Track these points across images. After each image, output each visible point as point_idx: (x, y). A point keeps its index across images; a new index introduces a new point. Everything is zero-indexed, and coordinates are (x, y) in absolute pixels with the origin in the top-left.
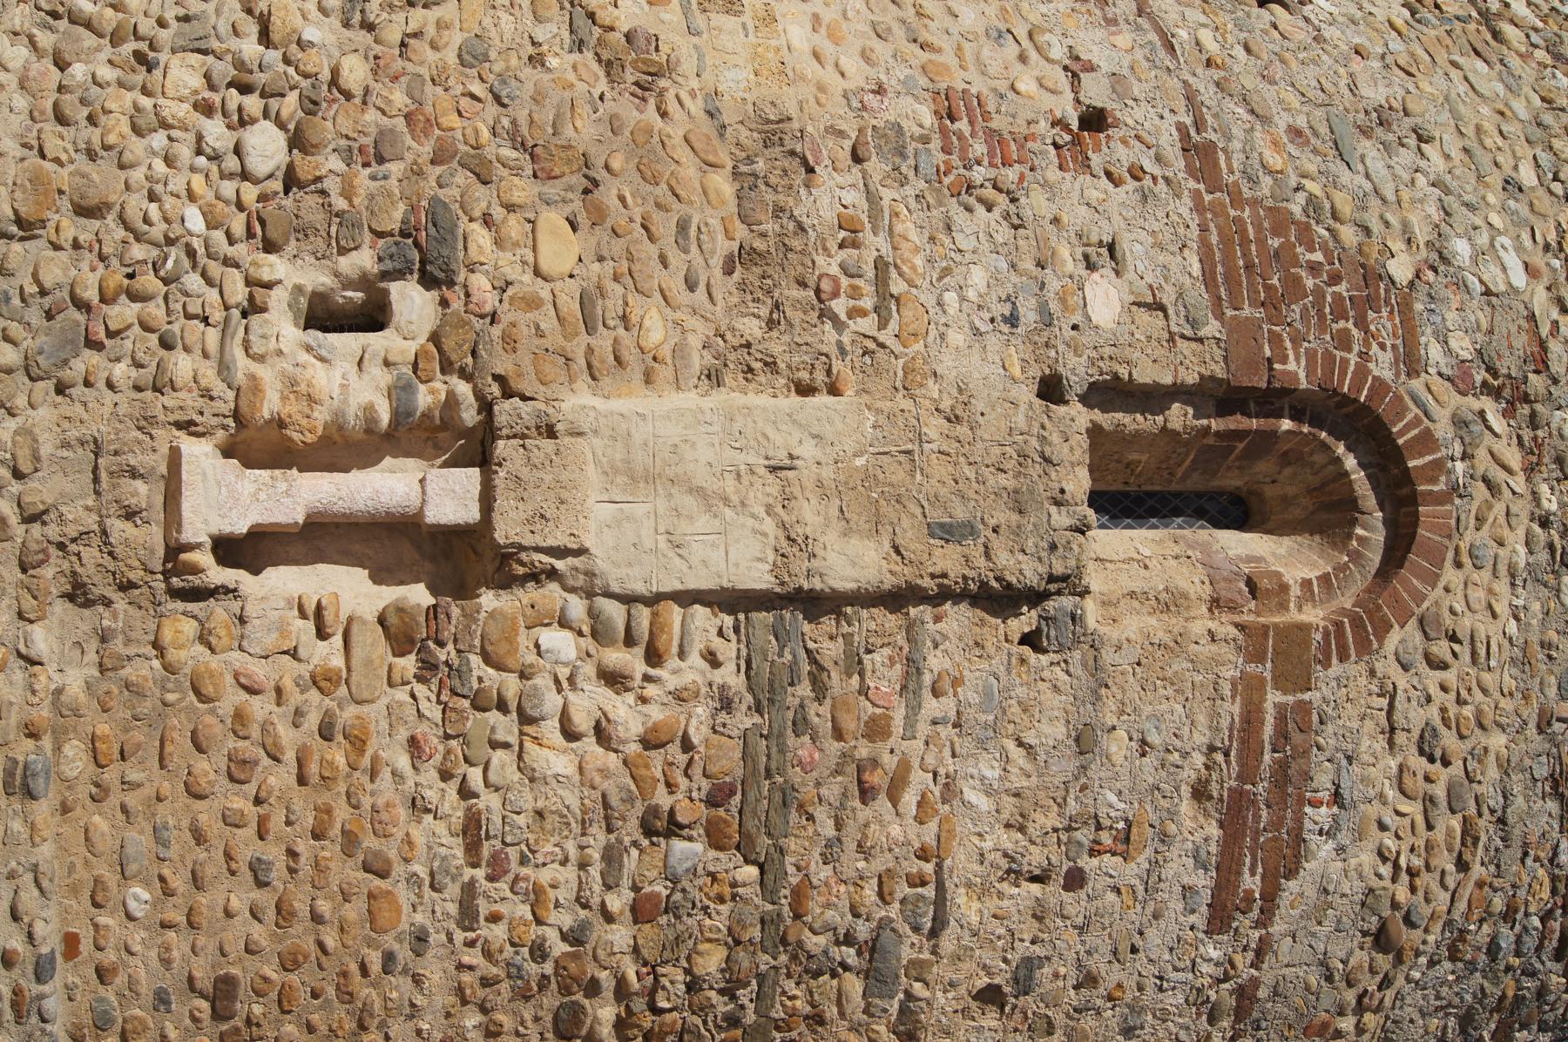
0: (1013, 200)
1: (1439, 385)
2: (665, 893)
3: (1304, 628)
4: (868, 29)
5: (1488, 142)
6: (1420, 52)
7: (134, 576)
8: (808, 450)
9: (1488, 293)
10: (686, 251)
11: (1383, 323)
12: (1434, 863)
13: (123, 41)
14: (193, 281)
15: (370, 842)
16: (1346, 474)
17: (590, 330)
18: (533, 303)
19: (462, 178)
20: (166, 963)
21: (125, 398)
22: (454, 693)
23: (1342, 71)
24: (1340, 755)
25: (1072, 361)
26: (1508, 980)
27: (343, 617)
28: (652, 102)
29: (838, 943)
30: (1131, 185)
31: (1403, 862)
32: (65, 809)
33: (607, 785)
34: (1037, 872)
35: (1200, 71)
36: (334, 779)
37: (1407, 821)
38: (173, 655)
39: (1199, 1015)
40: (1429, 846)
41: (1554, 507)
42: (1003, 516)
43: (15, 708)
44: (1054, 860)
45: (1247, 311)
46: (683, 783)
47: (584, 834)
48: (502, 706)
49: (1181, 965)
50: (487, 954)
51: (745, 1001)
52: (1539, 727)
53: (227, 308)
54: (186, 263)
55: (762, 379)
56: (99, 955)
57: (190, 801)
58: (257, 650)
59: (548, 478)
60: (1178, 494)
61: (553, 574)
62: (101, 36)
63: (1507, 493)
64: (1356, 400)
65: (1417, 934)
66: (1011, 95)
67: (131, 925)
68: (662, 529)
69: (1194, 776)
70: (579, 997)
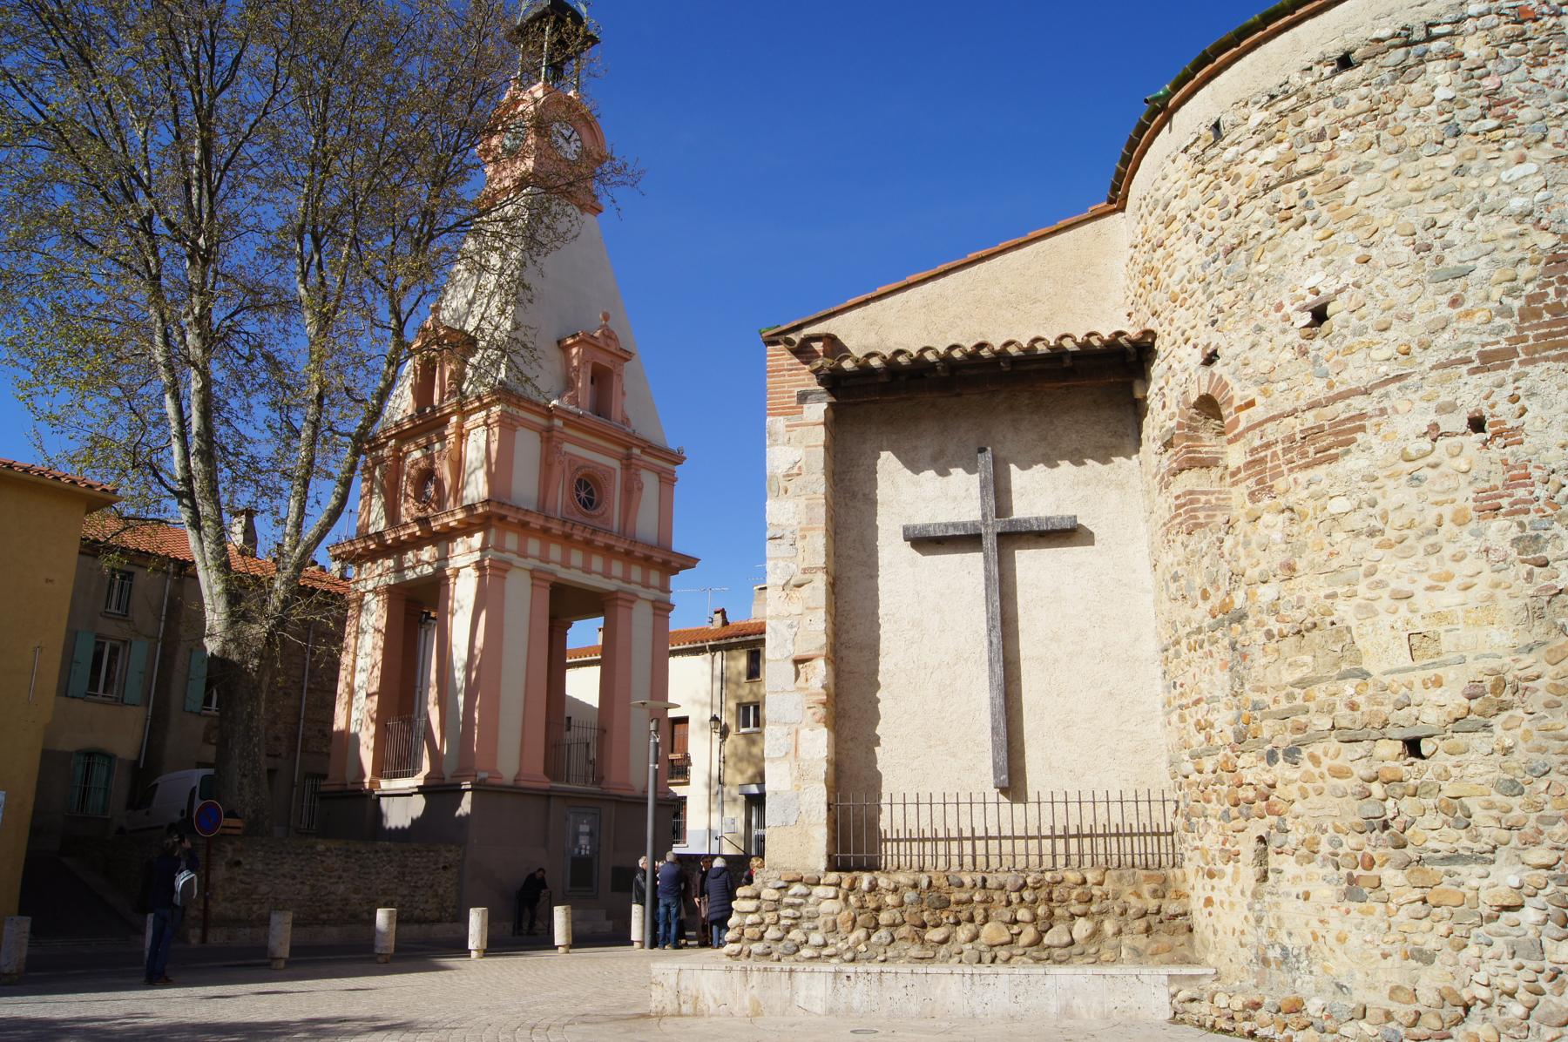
30: (1523, 401)
66: (1472, 473)
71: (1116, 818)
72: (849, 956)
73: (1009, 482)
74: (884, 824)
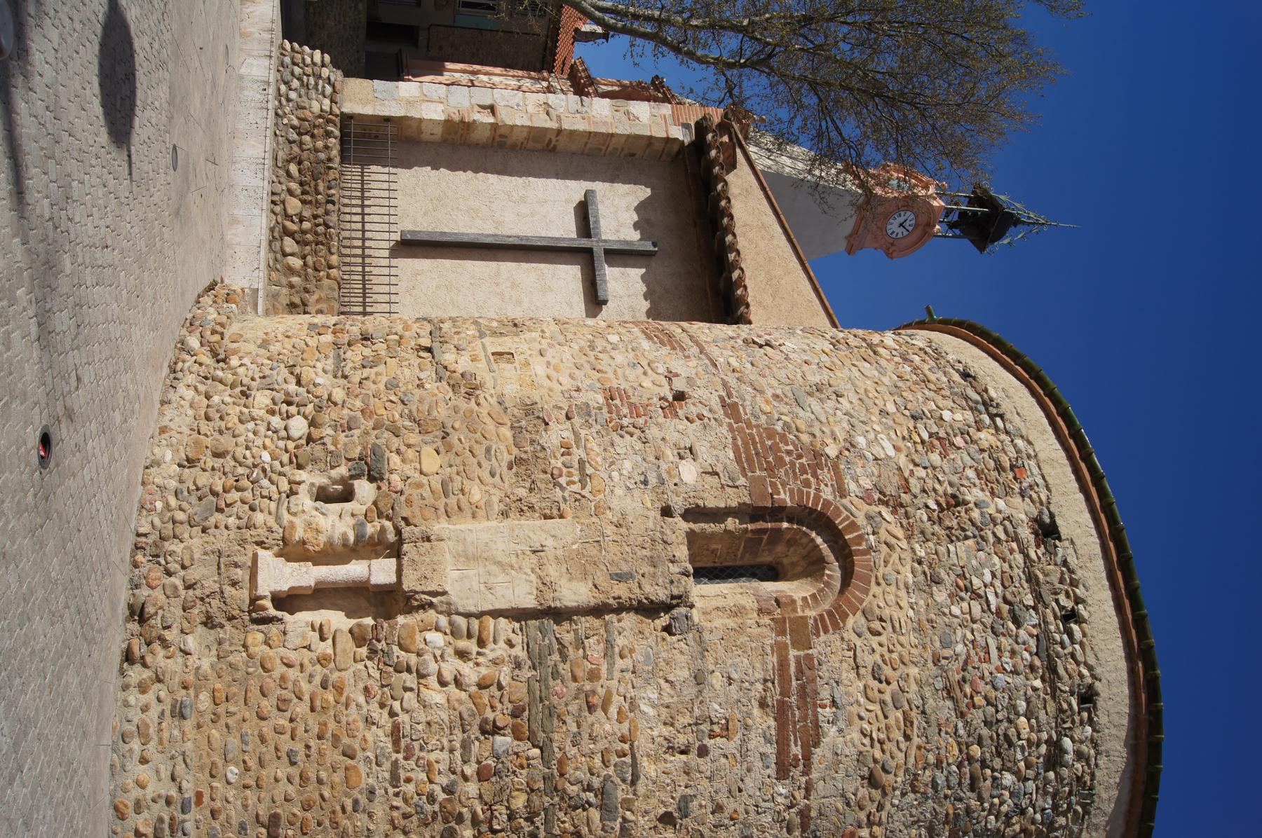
0: (643, 432)
1: (856, 501)
2: (494, 764)
3: (804, 618)
4: (573, 366)
5: (870, 395)
6: (836, 361)
7: (236, 613)
8: (550, 543)
9: (876, 459)
10: (490, 460)
11: (825, 474)
12: (891, 736)
13: (236, 387)
14: (265, 482)
15: (345, 740)
16: (818, 546)
17: (446, 496)
18: (419, 485)
19: (387, 434)
20: (245, 807)
21: (233, 534)
22: (385, 664)
23: (798, 370)
24: (832, 681)
25: (675, 499)
26: (948, 805)
27: (332, 630)
28: (473, 400)
29: (584, 791)
30: (698, 422)
31: (874, 736)
32: (199, 726)
33: (462, 708)
34: (683, 748)
35: (729, 374)
36: (328, 708)
37: (873, 714)
38: (252, 649)
39: (781, 828)
40: (887, 728)
41: (923, 554)
42: (646, 569)
43: (178, 674)
44: (690, 740)
45: (758, 473)
46: (499, 706)
47: (451, 734)
48: (409, 670)
49: (766, 798)
50: (405, 800)
51: (539, 824)
52: (933, 662)
53: (280, 493)
54: (262, 475)
55: (528, 514)
56: (212, 803)
57: (258, 721)
58: (292, 647)
59: (428, 560)
60: (741, 567)
61: (431, 605)
62: (226, 385)
63: (898, 549)
64: (816, 510)
65: (891, 777)
66: (639, 388)
67: (228, 787)
68: (482, 581)
69: (758, 695)
70: (453, 824)
71: (375, 280)
72: (280, 112)
73: (633, 267)
74: (374, 168)
